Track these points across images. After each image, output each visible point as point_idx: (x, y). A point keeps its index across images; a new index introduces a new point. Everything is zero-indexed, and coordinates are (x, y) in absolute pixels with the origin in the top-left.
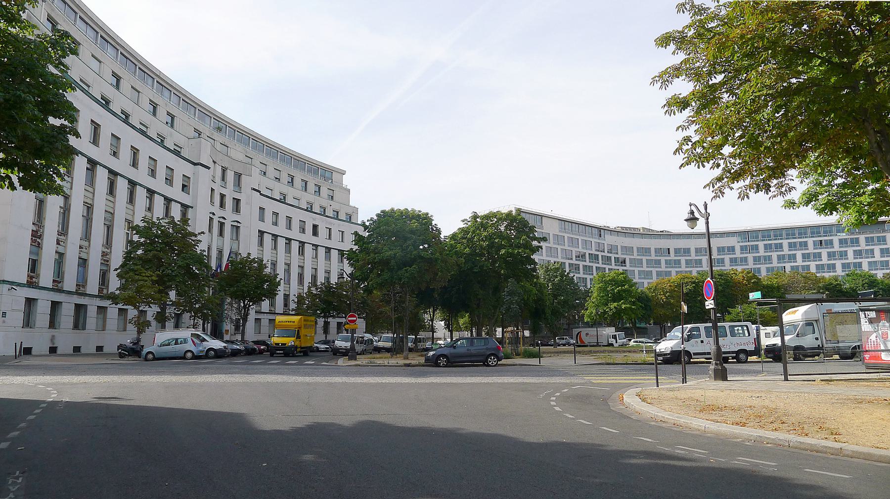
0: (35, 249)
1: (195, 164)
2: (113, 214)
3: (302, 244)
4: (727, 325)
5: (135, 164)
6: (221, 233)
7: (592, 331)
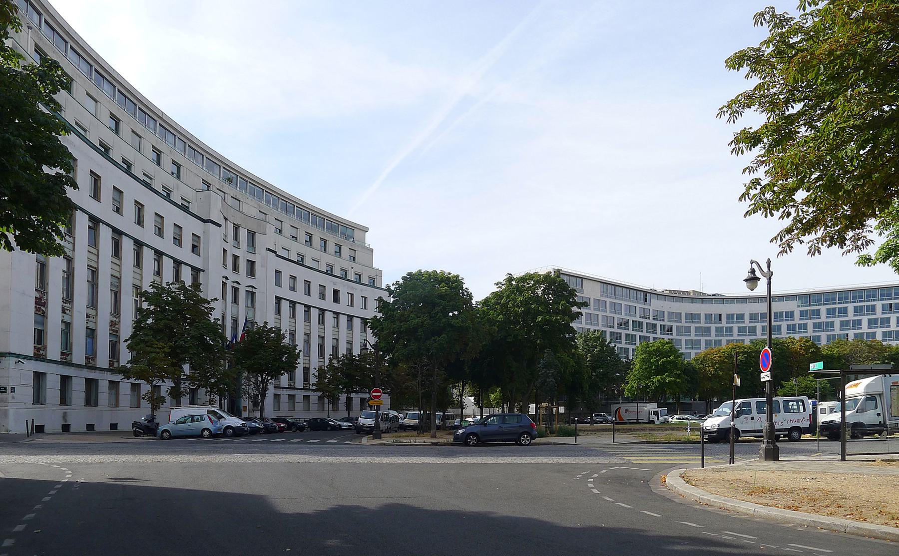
0: (40, 318)
1: (205, 221)
2: (119, 279)
3: (322, 311)
4: (780, 399)
5: (140, 222)
6: (235, 300)
7: (632, 407)
